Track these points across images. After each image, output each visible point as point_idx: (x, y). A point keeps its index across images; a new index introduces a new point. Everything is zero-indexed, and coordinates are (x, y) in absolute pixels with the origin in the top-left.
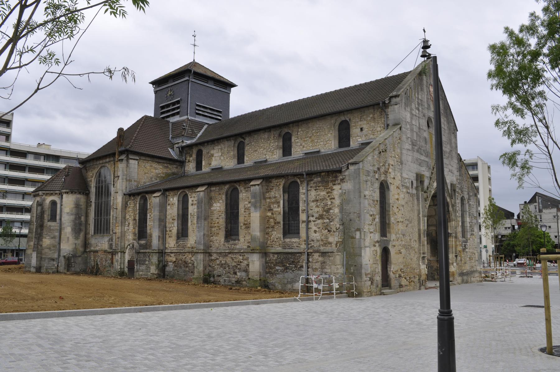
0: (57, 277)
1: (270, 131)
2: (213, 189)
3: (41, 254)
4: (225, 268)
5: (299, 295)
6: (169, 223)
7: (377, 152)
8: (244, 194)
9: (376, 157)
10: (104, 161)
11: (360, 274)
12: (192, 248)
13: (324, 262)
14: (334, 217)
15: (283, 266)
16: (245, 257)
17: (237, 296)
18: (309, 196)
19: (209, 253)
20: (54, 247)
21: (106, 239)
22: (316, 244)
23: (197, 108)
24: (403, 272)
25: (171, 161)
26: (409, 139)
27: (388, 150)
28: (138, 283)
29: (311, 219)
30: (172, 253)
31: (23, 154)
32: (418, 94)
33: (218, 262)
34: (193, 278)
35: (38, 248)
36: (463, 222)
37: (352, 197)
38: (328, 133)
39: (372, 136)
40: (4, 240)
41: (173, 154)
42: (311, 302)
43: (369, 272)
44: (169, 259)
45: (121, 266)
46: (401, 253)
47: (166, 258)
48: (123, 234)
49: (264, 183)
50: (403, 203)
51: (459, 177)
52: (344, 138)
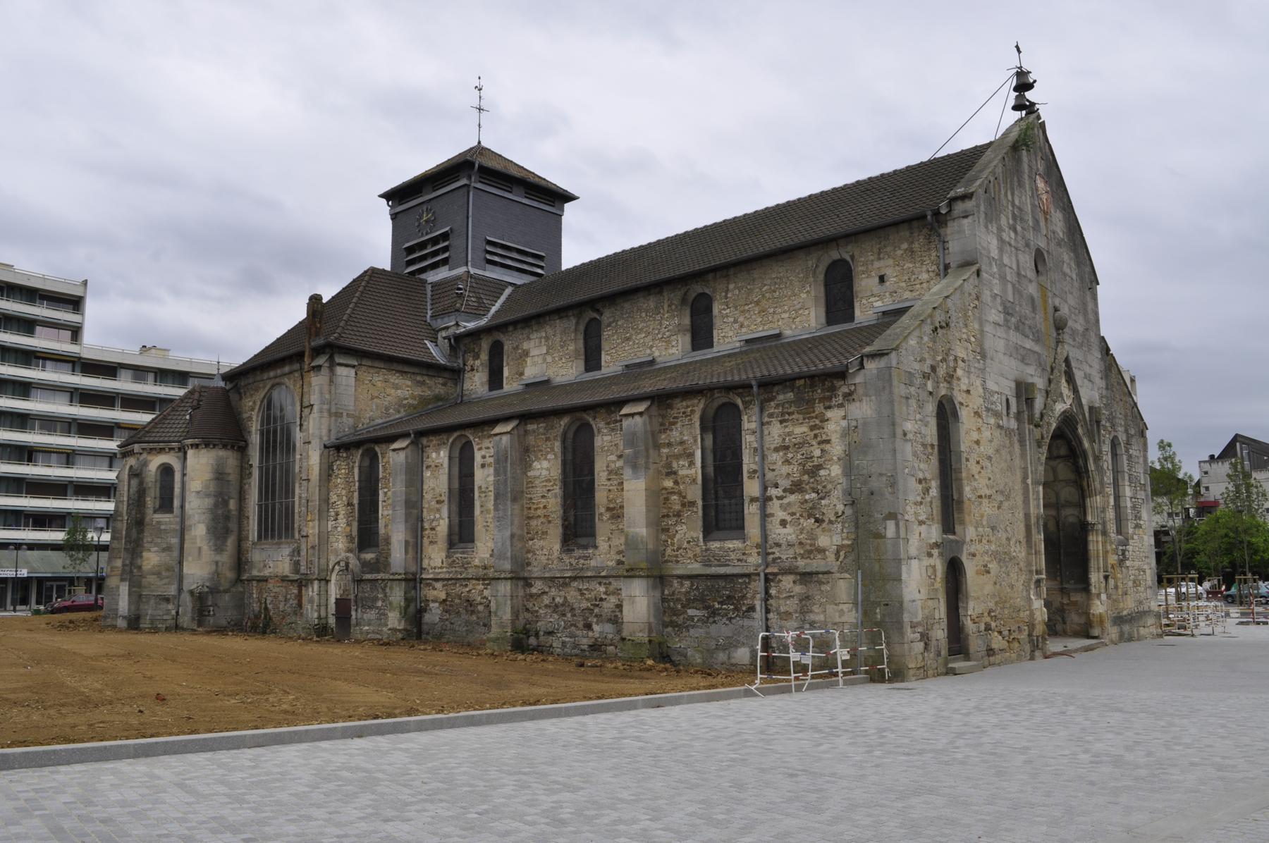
0: (173, 640)
1: (661, 292)
2: (530, 427)
3: (140, 586)
4: (564, 615)
5: (758, 681)
6: (430, 510)
7: (928, 329)
8: (606, 438)
9: (926, 339)
10: (279, 372)
11: (899, 625)
12: (485, 568)
13: (808, 598)
14: (829, 486)
15: (706, 608)
16: (611, 588)
17: (604, 686)
18: (765, 436)
19: (525, 579)
20: (167, 570)
21: (286, 551)
22: (785, 555)
23: (489, 248)
24: (995, 618)
25: (431, 368)
26: (998, 300)
27: (952, 325)
28: (357, 652)
29: (772, 492)
30: (437, 580)
31: (108, 369)
32: (1013, 195)
33: (546, 600)
34: (489, 640)
35: (132, 573)
36: (1117, 498)
37: (874, 436)
38: (801, 292)
39: (907, 295)
40: (71, 556)
41: (437, 352)
42: (786, 696)
43: (919, 618)
44: (431, 594)
45: (319, 612)
46: (988, 572)
47: (424, 592)
48: (324, 538)
49: (654, 410)
50: (991, 452)
51: (1104, 392)
52: (839, 302)
